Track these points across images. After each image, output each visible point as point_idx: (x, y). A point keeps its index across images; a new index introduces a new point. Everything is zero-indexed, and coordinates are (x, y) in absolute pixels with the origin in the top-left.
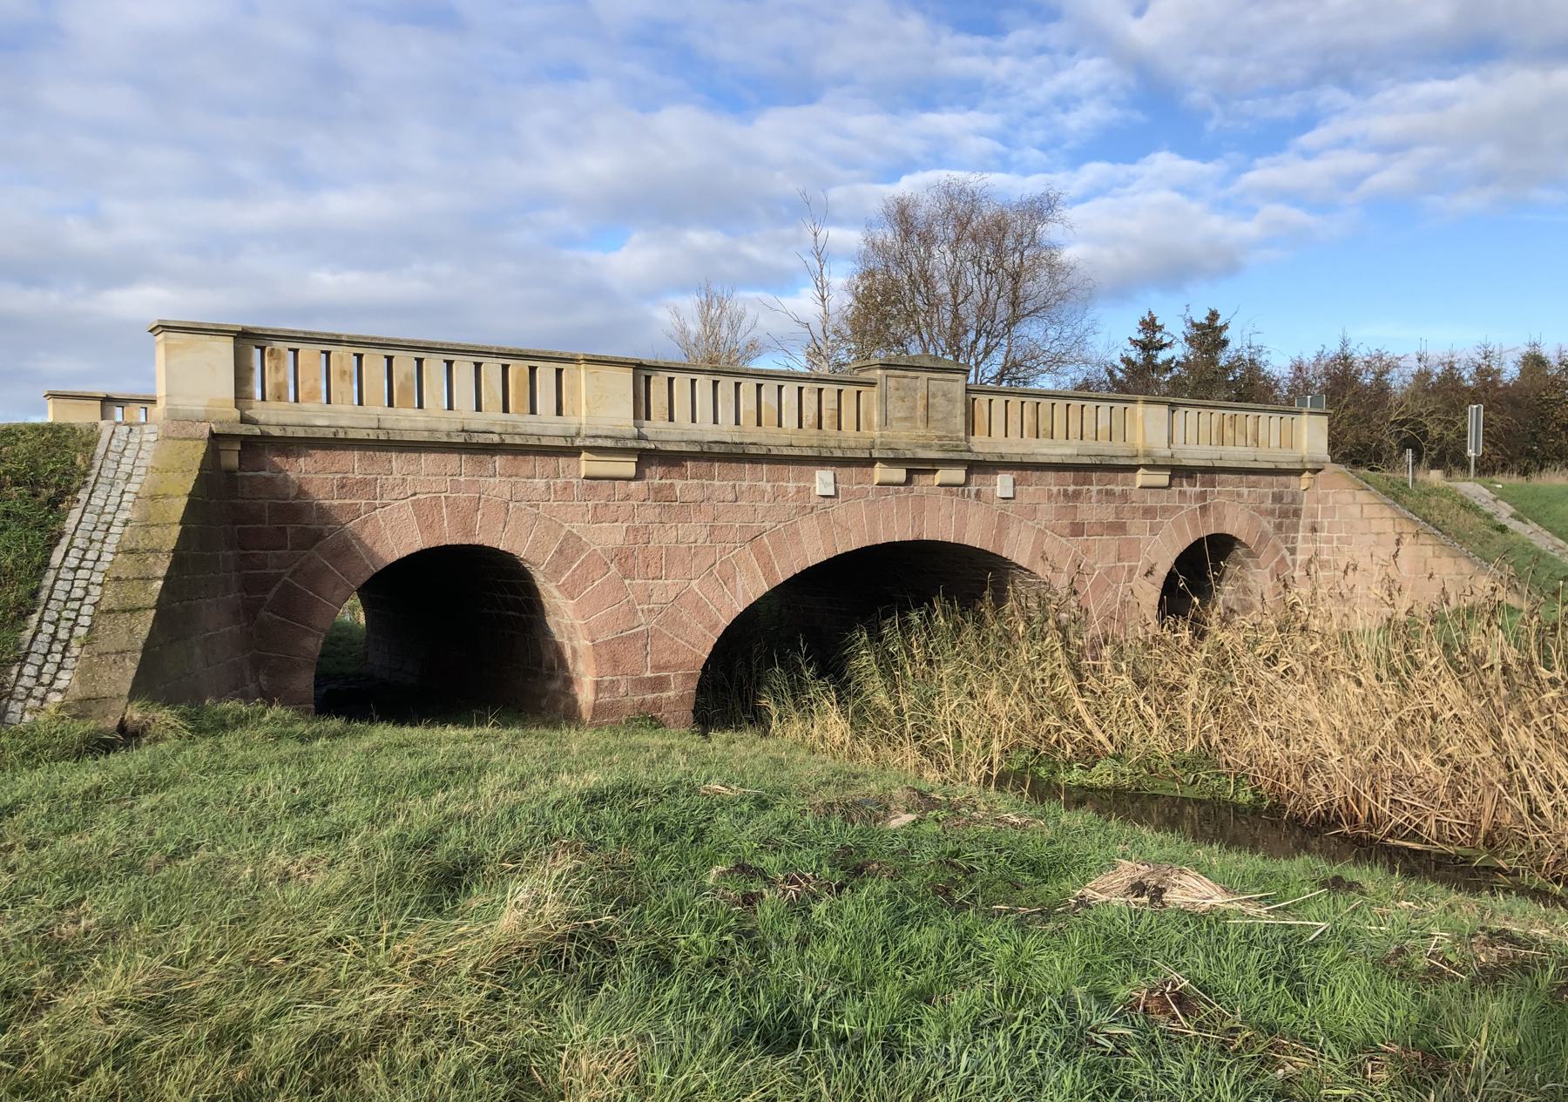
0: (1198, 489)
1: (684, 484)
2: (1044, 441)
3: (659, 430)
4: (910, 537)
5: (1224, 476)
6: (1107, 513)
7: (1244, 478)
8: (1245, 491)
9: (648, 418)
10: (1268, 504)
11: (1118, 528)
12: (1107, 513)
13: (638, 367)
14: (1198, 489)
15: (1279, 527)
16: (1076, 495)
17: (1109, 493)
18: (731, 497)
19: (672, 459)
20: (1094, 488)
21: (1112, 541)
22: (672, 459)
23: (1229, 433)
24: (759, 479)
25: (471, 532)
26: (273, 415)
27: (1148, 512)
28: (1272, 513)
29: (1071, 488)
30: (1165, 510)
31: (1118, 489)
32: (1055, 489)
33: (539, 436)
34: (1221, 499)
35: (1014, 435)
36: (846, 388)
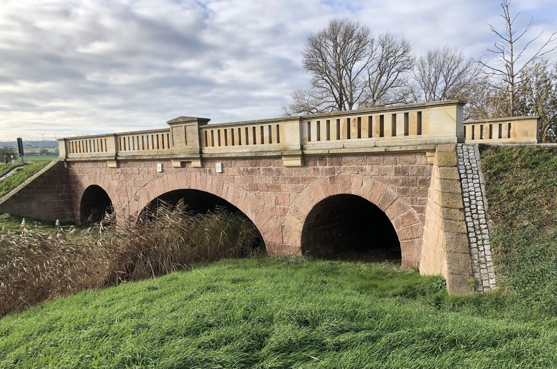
0: (327, 167)
1: (133, 168)
2: (237, 146)
3: (123, 154)
4: (186, 188)
5: (349, 158)
6: (269, 180)
7: (368, 159)
8: (368, 167)
9: (207, 146)
10: (392, 176)
11: (277, 188)
12: (269, 180)
13: (115, 135)
14: (327, 167)
15: (404, 192)
16: (251, 172)
17: (270, 170)
18: (138, 173)
19: (125, 161)
20: (261, 168)
21: (271, 195)
22: (125, 161)
23: (354, 130)
24: (143, 167)
25: (95, 182)
26: (73, 156)
27: (292, 180)
28: (396, 181)
29: (249, 168)
30: (304, 179)
31: (274, 168)
32: (242, 169)
33: (401, 146)
34: (347, 173)
35: (156, 149)
36: (241, 127)
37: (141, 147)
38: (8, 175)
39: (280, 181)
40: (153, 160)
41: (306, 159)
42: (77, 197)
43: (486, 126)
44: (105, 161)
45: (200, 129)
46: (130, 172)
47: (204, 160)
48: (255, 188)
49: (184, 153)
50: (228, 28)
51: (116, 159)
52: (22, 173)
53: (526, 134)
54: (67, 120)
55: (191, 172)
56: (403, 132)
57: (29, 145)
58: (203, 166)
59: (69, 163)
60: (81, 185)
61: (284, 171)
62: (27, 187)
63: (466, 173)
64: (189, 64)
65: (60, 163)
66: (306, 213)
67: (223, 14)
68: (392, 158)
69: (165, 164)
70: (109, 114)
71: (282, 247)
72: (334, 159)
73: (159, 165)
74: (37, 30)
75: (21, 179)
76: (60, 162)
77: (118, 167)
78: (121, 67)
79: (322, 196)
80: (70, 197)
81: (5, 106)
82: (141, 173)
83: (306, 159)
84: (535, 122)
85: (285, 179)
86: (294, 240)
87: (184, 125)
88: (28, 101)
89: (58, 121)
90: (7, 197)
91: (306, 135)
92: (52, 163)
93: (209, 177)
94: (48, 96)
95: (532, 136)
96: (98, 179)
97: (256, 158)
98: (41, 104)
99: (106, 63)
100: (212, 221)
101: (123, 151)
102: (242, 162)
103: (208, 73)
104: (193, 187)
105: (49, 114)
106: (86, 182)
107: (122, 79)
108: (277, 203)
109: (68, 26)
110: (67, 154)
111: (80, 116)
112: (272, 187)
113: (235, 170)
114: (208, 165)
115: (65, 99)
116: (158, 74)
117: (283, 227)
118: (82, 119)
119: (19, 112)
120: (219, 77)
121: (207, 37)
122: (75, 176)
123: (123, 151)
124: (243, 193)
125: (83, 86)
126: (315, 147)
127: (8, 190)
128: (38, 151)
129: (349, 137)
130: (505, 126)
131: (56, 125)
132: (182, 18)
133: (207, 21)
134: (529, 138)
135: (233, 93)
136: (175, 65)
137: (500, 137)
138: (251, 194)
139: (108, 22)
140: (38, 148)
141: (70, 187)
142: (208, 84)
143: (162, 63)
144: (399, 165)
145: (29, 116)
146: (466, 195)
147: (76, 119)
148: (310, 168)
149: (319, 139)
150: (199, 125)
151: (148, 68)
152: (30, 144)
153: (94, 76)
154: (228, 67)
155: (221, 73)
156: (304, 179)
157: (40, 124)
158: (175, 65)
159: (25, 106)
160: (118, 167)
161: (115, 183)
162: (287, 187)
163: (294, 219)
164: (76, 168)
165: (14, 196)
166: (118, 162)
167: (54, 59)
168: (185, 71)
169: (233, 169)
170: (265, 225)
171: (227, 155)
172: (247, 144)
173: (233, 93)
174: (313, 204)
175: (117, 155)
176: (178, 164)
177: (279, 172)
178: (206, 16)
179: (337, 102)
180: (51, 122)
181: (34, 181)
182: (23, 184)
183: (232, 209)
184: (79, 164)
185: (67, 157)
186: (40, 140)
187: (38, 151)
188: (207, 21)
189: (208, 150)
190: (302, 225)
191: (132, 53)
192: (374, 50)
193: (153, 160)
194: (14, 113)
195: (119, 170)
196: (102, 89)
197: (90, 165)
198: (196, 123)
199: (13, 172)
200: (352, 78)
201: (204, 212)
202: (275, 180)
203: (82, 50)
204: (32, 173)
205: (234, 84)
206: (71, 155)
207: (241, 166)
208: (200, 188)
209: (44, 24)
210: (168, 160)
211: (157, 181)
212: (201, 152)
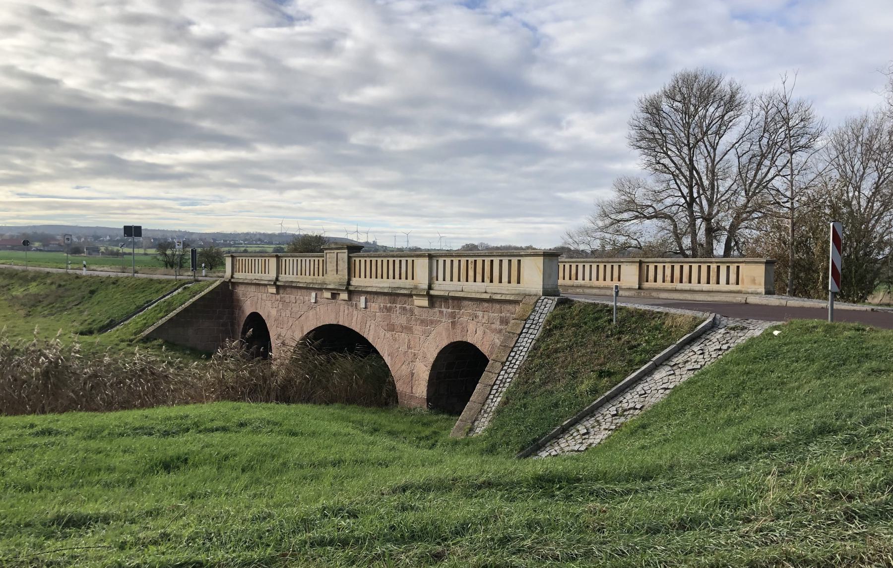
3: (283, 278)
4: (335, 323)
8: (480, 314)
11: (408, 329)
14: (450, 310)
17: (404, 309)
24: (299, 295)
26: (239, 276)
28: (500, 331)
29: (388, 305)
30: (432, 322)
31: (408, 307)
32: (382, 305)
37: (299, 273)
38: (175, 293)
39: (413, 323)
40: (308, 288)
41: (433, 300)
42: (239, 325)
43: (714, 267)
44: (266, 285)
45: (349, 258)
46: (287, 301)
47: (351, 293)
48: (391, 328)
49: (334, 283)
50: (572, 62)
51: (275, 283)
52: (187, 293)
53: (753, 281)
54: (318, 204)
55: (340, 305)
56: (507, 280)
57: (260, 240)
58: (350, 299)
59: (234, 284)
60: (243, 312)
61: (416, 311)
62: (186, 310)
63: (529, 328)
64: (508, 120)
65: (225, 284)
66: (432, 360)
67: (565, 39)
68: (498, 306)
69: (319, 293)
70: (381, 195)
71: (412, 397)
72: (456, 302)
73: (313, 294)
74: (288, 71)
75: (183, 300)
76: (224, 282)
77: (278, 293)
78: (404, 124)
79: (445, 343)
80: (233, 324)
81: (234, 181)
82: (298, 302)
83: (433, 300)
84: (763, 267)
85: (416, 320)
86: (421, 390)
87: (336, 251)
88: (265, 173)
89: (305, 204)
90: (164, 320)
91: (434, 274)
92: (218, 283)
93: (355, 312)
94: (294, 166)
95: (760, 284)
96: (259, 306)
97: (393, 295)
98: (284, 178)
99: (380, 117)
100: (345, 364)
101: (283, 275)
102: (383, 298)
103: (537, 134)
104: (341, 323)
105: (294, 194)
106: (248, 309)
107: (404, 142)
108: (409, 347)
109: (329, 64)
110: (233, 273)
112: (406, 328)
113: (377, 306)
114: (355, 298)
115: (318, 172)
116: (457, 135)
117: (413, 374)
118: (341, 202)
120: (556, 139)
121: (538, 77)
122: (238, 301)
123: (283, 275)
124: (382, 333)
125: (345, 152)
126: (442, 287)
127: (167, 312)
129: (467, 281)
130: (733, 268)
131: (301, 210)
132: (498, 44)
133: (536, 51)
134: (756, 287)
135: (576, 165)
136: (484, 120)
137: (728, 283)
138: (389, 335)
139: (386, 57)
140: (272, 244)
141: (233, 313)
142: (537, 151)
143: (464, 118)
144: (503, 315)
145: (266, 196)
146: (515, 349)
147: (331, 202)
148: (437, 310)
149: (444, 280)
150: (349, 253)
151: (445, 125)
152: (262, 238)
153: (360, 137)
154: (570, 124)
155: (559, 133)
156: (432, 322)
157: (280, 208)
158: (484, 120)
159: (260, 182)
160: (278, 293)
161: (274, 312)
162: (418, 329)
163: (422, 365)
164: (240, 290)
165: (171, 319)
166: (278, 288)
167: (306, 112)
168: (500, 130)
169: (376, 305)
170: (397, 369)
171: (369, 289)
172: (388, 278)
173: (576, 165)
174: (438, 351)
175: (277, 279)
176: (328, 295)
177: (412, 311)
178: (537, 43)
179: (685, 198)
180: (294, 206)
181: (194, 304)
183: (369, 349)
184: (243, 286)
185: (232, 277)
186: (277, 232)
188: (536, 51)
189: (355, 282)
190: (428, 373)
191: (417, 101)
192: (754, 116)
193: (308, 288)
194: (246, 191)
195: (278, 297)
196: (373, 157)
197: (253, 288)
198: (346, 251)
199: (180, 290)
200: (717, 159)
201: (341, 351)
202: (409, 321)
203: (346, 98)
204: (196, 293)
205: (580, 151)
206: (236, 275)
207: (381, 302)
208: (346, 325)
209: (298, 62)
210: (321, 289)
211: (311, 313)
212: (349, 284)
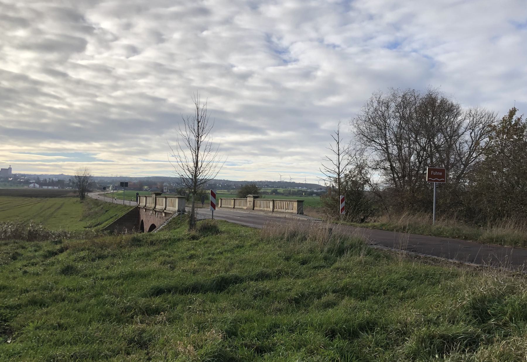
45: (254, 201)
59: (139, 208)
74: (286, 90)
94: (288, 143)
98: (283, 150)
105: (289, 158)
111: (313, 160)
119: (266, 157)
128: (269, 191)
131: (293, 167)
145: (273, 160)
147: (309, 163)
157: (281, 167)
159: (270, 152)
180: (289, 165)
182: (50, 187)
186: (277, 181)
187: (269, 191)
194: (262, 157)
206: (168, 208)
209: (291, 84)
